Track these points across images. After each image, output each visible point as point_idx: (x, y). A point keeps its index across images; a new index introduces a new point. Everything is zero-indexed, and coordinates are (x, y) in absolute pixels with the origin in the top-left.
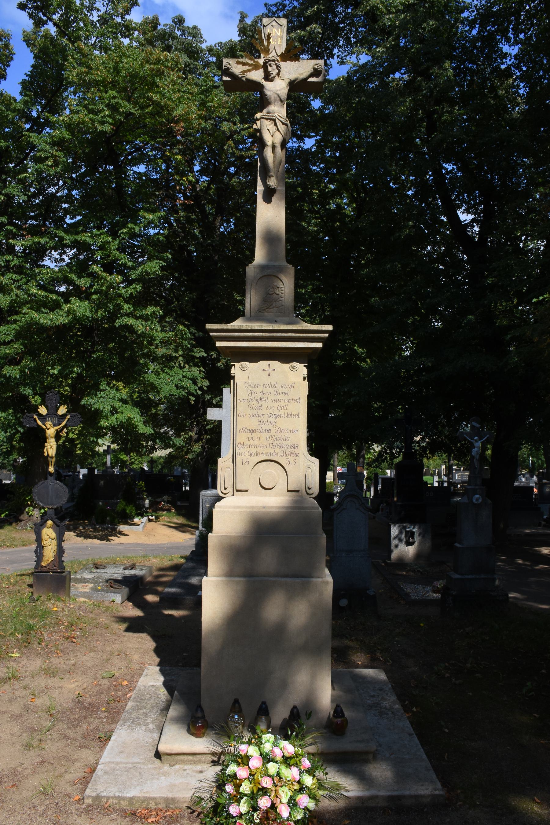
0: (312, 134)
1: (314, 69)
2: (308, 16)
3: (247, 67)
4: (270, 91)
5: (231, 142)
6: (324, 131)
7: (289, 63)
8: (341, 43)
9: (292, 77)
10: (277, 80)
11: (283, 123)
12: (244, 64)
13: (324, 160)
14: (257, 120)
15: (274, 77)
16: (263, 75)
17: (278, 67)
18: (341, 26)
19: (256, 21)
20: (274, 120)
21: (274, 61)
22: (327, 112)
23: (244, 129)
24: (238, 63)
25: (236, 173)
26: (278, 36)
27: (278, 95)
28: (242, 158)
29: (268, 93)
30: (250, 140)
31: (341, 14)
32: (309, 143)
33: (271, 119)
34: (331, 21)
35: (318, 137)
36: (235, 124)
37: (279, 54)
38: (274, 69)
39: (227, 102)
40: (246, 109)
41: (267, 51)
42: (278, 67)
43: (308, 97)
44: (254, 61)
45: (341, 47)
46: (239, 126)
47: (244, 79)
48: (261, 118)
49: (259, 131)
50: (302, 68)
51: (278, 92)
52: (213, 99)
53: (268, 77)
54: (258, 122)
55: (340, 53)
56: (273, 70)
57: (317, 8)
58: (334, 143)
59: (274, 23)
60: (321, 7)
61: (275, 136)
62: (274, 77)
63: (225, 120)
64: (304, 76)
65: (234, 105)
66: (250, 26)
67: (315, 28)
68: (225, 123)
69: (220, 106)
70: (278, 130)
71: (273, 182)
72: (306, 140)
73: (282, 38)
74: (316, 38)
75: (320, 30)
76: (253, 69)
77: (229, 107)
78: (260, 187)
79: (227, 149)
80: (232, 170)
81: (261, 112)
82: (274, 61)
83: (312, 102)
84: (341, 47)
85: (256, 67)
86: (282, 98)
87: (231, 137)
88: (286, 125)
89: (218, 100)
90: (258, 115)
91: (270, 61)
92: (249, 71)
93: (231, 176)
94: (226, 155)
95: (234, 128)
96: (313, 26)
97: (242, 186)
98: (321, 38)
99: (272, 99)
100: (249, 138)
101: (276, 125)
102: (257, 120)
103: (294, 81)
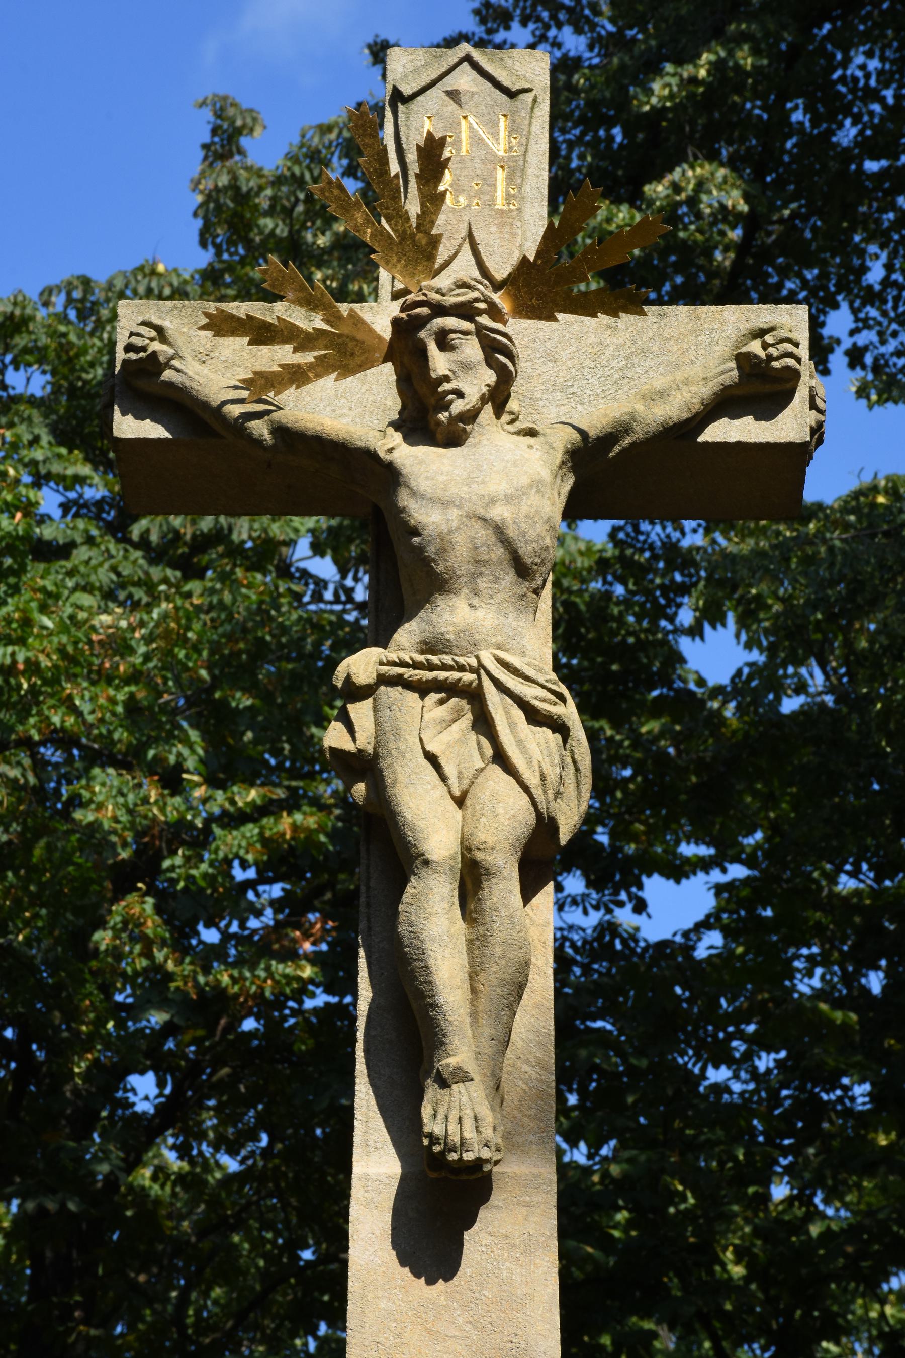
0: (688, 850)
1: (744, 360)
2: (658, 113)
3: (281, 355)
4: (446, 504)
5: (142, 907)
6: (774, 830)
7: (568, 322)
8: (875, 275)
9: (596, 417)
10: (491, 438)
11: (534, 716)
12: (263, 334)
13: (784, 1022)
14: (356, 692)
15: (471, 416)
16: (392, 404)
17: (496, 350)
18: (872, 166)
19: (315, 157)
20: (475, 697)
21: (465, 311)
22: (790, 705)
23: (234, 819)
24: (222, 326)
25: (173, 1114)
26: (492, 160)
27: (499, 530)
28: (212, 1006)
29: (426, 515)
30: (276, 890)
31: (874, 95)
32: (674, 908)
33: (451, 690)
34: (807, 143)
35: (737, 871)
36: (172, 780)
37: (501, 272)
38: (467, 367)
39: (119, 645)
40: (252, 688)
41: (421, 250)
42: (496, 350)
43: (659, 612)
44: (333, 318)
45: (871, 297)
46: (203, 799)
47: (260, 429)
48: (384, 680)
49: (365, 766)
50: (651, 364)
51: (498, 512)
52: (27, 622)
53: (426, 416)
54: (361, 712)
55: (867, 337)
56: (464, 372)
57: (717, 67)
58: (847, 905)
59: (464, 79)
60: (746, 60)
61: (481, 796)
62: (471, 416)
63: (105, 756)
64: (673, 409)
65: (169, 664)
66: (278, 181)
67: (701, 185)
68: (104, 782)
69: (71, 661)
70: (501, 758)
71: (460, 1116)
72: (655, 887)
73: (516, 171)
74: (708, 253)
75: (735, 200)
76: (322, 367)
77: (135, 677)
78: (376, 1167)
79: (117, 954)
80: (144, 1090)
81: (383, 641)
82: (465, 311)
83: (685, 645)
84: (871, 297)
85: (345, 353)
86: (526, 551)
87: (143, 869)
88: (560, 728)
89: (63, 628)
90: (361, 665)
91: (440, 310)
92: (296, 376)
93: (140, 1134)
94: (107, 990)
95: (167, 809)
96: (687, 175)
97: (214, 1203)
98: (742, 248)
99: (458, 559)
100: (263, 879)
101: (484, 724)
102: (356, 692)
103: (609, 438)
